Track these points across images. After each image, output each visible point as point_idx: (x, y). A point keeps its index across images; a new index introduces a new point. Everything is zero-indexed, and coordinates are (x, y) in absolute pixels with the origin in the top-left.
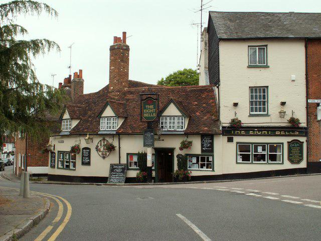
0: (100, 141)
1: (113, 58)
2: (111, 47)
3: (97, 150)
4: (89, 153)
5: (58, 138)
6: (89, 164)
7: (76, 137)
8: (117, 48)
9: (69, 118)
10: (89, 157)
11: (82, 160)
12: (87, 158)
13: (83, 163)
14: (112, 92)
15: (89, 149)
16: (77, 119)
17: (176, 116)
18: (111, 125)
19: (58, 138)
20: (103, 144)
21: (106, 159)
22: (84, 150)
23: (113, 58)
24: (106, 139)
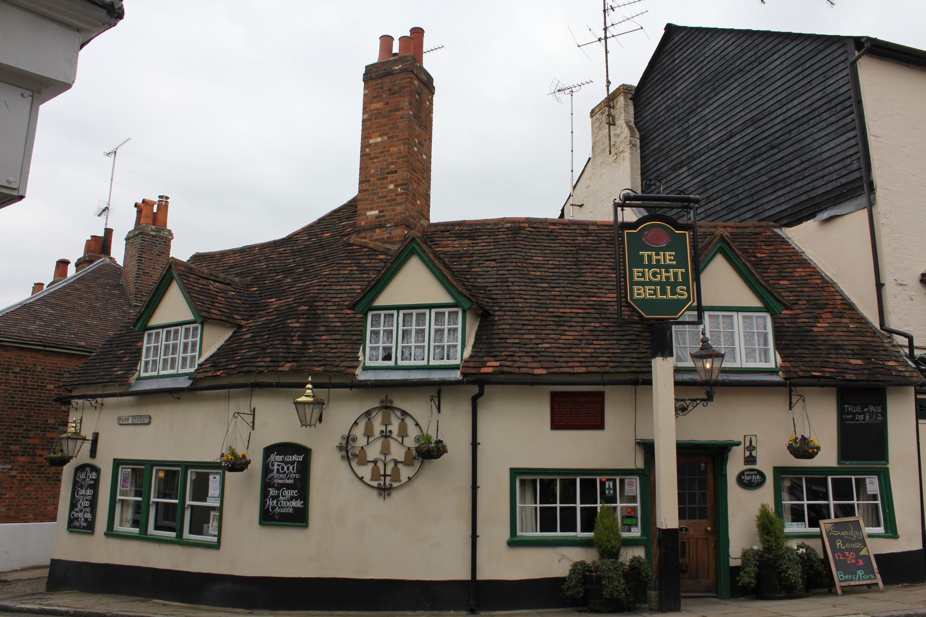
0: (368, 414)
1: (378, 105)
2: (369, 69)
3: (347, 458)
4: (304, 468)
5: (118, 406)
6: (299, 518)
7: (228, 397)
8: (403, 71)
9: (190, 317)
10: (302, 487)
11: (263, 503)
12: (288, 493)
13: (268, 518)
14: (373, 228)
15: (305, 451)
16: (221, 322)
17: (430, 307)
18: (180, 355)
19: (125, 408)
20: (378, 427)
21: (396, 495)
22: (276, 458)
23: (378, 105)
24: (398, 403)
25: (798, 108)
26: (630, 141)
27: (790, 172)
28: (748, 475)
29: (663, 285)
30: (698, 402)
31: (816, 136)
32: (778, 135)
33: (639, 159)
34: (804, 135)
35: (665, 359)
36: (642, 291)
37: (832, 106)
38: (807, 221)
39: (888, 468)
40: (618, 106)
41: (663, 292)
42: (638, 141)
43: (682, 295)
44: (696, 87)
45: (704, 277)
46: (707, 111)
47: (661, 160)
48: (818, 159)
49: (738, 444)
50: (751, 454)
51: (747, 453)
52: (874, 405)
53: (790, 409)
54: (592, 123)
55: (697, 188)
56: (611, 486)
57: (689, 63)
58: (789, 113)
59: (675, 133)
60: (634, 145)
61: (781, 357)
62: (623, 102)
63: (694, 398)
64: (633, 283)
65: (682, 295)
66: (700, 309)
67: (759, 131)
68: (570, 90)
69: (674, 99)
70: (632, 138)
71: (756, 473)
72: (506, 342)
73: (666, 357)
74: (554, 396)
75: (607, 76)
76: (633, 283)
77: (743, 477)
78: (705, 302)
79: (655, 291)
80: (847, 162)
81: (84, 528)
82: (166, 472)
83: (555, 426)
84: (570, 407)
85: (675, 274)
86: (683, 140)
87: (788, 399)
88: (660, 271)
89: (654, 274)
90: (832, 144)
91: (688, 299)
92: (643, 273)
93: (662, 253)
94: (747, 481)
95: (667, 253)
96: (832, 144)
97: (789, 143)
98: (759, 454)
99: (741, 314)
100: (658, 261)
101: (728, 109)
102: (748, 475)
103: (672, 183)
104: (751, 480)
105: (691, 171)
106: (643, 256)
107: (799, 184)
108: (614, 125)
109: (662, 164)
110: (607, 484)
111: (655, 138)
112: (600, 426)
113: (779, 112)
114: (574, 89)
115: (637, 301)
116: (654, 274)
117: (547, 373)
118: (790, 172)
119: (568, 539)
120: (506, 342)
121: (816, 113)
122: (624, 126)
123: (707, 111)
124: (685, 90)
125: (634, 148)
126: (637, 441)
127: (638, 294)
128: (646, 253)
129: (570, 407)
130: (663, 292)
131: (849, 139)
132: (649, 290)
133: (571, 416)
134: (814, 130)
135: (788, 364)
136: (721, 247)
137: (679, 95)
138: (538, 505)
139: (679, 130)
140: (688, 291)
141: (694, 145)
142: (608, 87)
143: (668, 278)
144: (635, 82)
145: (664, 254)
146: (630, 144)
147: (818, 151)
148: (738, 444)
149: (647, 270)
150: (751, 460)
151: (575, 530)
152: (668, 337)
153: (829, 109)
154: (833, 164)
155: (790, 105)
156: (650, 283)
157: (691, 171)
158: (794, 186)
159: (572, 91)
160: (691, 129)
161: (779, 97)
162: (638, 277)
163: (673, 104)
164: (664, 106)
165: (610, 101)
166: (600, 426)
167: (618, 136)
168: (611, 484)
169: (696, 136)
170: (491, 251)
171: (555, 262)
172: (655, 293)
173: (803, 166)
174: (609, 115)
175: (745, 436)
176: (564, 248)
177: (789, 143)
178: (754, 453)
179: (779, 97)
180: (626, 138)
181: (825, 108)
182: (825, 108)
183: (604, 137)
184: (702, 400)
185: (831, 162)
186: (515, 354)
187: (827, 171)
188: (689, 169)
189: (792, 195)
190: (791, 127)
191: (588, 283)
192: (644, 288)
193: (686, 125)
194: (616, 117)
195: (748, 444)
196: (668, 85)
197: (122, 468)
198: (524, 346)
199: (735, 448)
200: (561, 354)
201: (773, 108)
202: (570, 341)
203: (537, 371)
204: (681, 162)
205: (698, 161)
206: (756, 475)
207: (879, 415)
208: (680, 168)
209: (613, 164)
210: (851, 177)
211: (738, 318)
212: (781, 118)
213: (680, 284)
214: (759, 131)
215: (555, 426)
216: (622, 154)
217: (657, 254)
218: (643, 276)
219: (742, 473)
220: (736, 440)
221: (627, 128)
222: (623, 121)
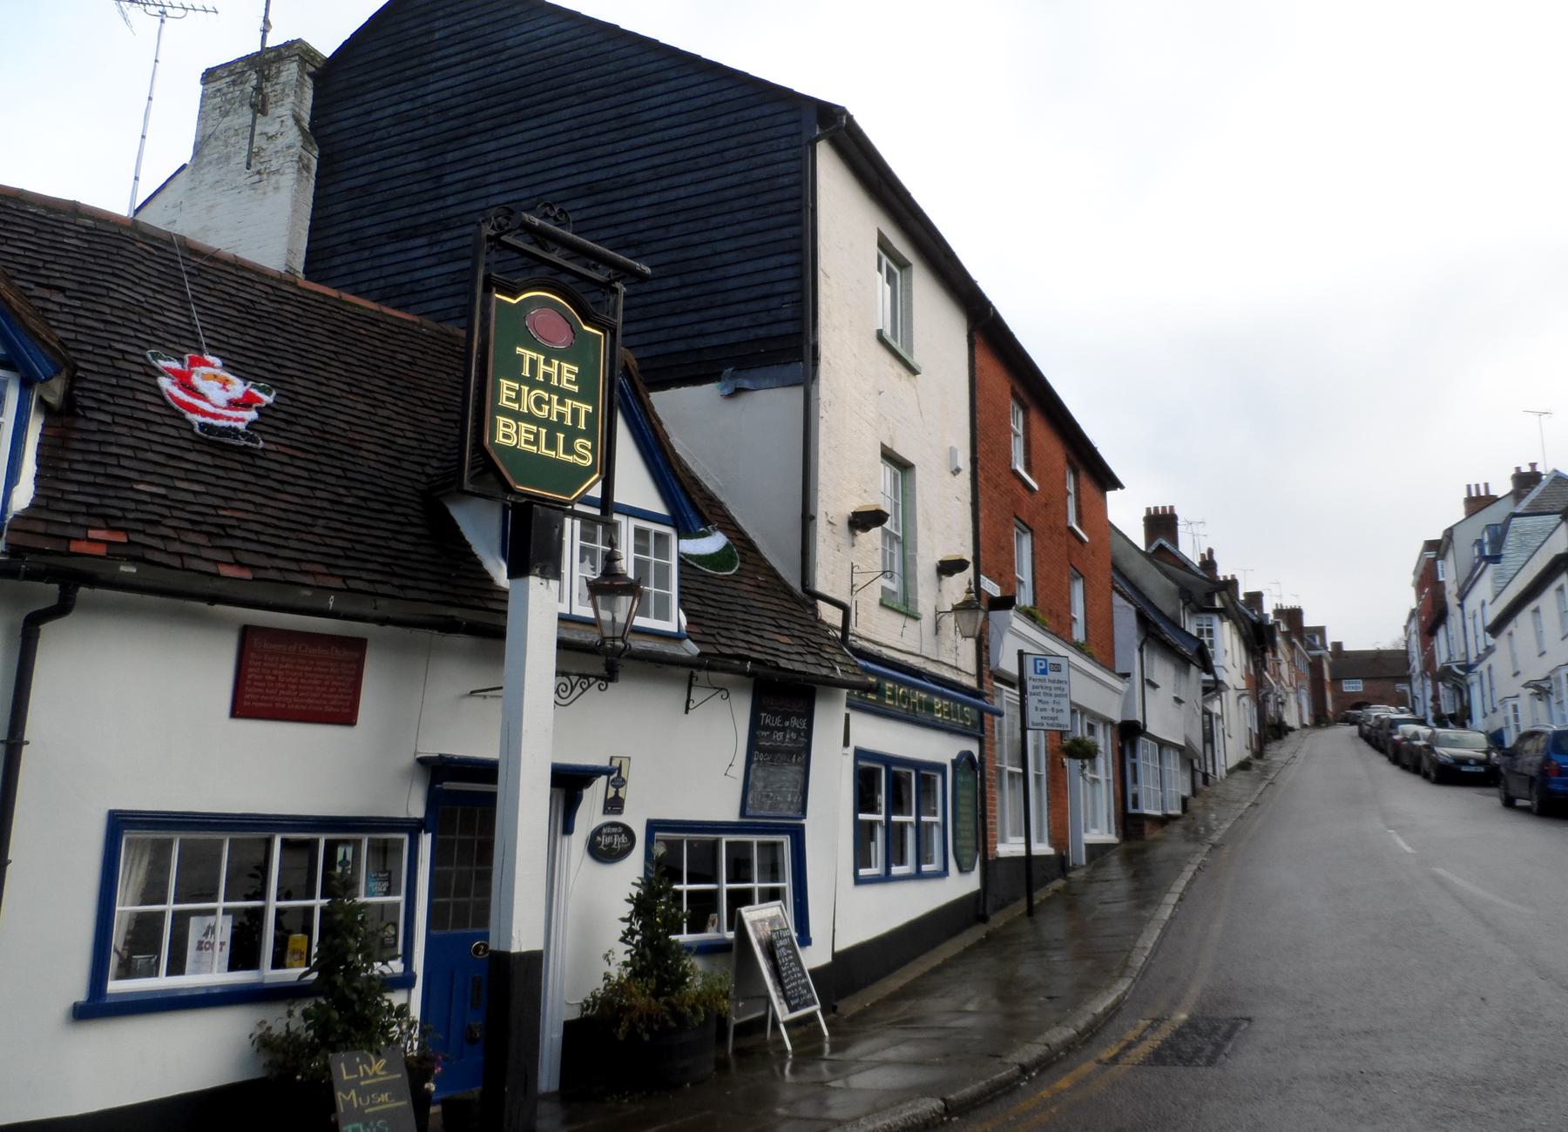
25: (692, 190)
26: (300, 157)
27: (657, 297)
28: (608, 835)
29: (553, 427)
30: (592, 680)
31: (719, 247)
32: (641, 226)
33: (312, 199)
34: (696, 238)
35: (544, 581)
36: (512, 431)
37: (758, 203)
38: (679, 386)
39: (803, 826)
40: (282, 79)
42: (315, 162)
43: (584, 458)
44: (473, 96)
46: (493, 145)
47: (364, 212)
48: (720, 286)
50: (617, 792)
51: (611, 793)
52: (798, 718)
53: (687, 712)
54: (203, 95)
55: (443, 283)
56: (349, 857)
57: (464, 46)
58: (672, 195)
59: (409, 168)
60: (307, 168)
62: (296, 76)
63: (587, 672)
65: (584, 458)
67: (603, 209)
68: (161, 8)
69: (418, 104)
70: (305, 153)
71: (620, 830)
72: (132, 489)
73: (547, 579)
74: (247, 635)
75: (267, 10)
77: (599, 838)
79: (537, 435)
80: (774, 302)
81: (940, 1064)
83: (242, 708)
85: (575, 412)
86: (426, 185)
87: (686, 693)
89: (539, 402)
90: (749, 267)
92: (519, 393)
93: (556, 362)
95: (566, 366)
96: (749, 267)
97: (662, 245)
98: (629, 794)
100: (547, 376)
101: (542, 153)
102: (608, 835)
103: (386, 260)
104: (611, 844)
105: (436, 249)
107: (672, 321)
108: (264, 113)
109: (367, 221)
110: (340, 851)
111: (357, 166)
112: (347, 717)
113: (650, 186)
114: (169, 11)
117: (254, 579)
118: (657, 297)
119: (197, 993)
120: (132, 489)
121: (726, 207)
122: (290, 122)
123: (493, 145)
124: (447, 93)
125: (305, 174)
127: (506, 436)
128: (528, 354)
130: (551, 444)
131: (783, 266)
134: (716, 234)
135: (696, 629)
137: (430, 99)
138: (221, 904)
139: (418, 166)
141: (450, 201)
142: (265, 32)
143: (561, 416)
144: (327, 46)
146: (297, 162)
147: (720, 272)
150: (614, 804)
152: (556, 538)
153: (753, 207)
154: (746, 301)
155: (677, 180)
156: (529, 418)
157: (436, 249)
158: (661, 322)
159: (163, 13)
160: (448, 169)
161: (657, 161)
163: (415, 112)
164: (390, 111)
165: (264, 63)
166: (347, 717)
167: (270, 138)
168: (350, 851)
169: (459, 187)
170: (48, 266)
172: (536, 442)
173: (684, 292)
174: (258, 89)
177: (662, 245)
179: (657, 161)
180: (289, 147)
181: (744, 202)
182: (744, 202)
183: (231, 132)
184: (598, 678)
185: (742, 295)
187: (733, 309)
188: (430, 245)
189: (655, 337)
190: (672, 219)
193: (438, 160)
194: (272, 100)
196: (408, 73)
201: (640, 176)
204: (415, 227)
205: (456, 233)
206: (620, 835)
207: (802, 734)
208: (411, 237)
209: (248, 192)
210: (776, 330)
212: (654, 198)
213: (583, 434)
214: (603, 209)
215: (242, 708)
216: (274, 178)
218: (518, 399)
219: (597, 832)
221: (296, 129)
222: (289, 112)
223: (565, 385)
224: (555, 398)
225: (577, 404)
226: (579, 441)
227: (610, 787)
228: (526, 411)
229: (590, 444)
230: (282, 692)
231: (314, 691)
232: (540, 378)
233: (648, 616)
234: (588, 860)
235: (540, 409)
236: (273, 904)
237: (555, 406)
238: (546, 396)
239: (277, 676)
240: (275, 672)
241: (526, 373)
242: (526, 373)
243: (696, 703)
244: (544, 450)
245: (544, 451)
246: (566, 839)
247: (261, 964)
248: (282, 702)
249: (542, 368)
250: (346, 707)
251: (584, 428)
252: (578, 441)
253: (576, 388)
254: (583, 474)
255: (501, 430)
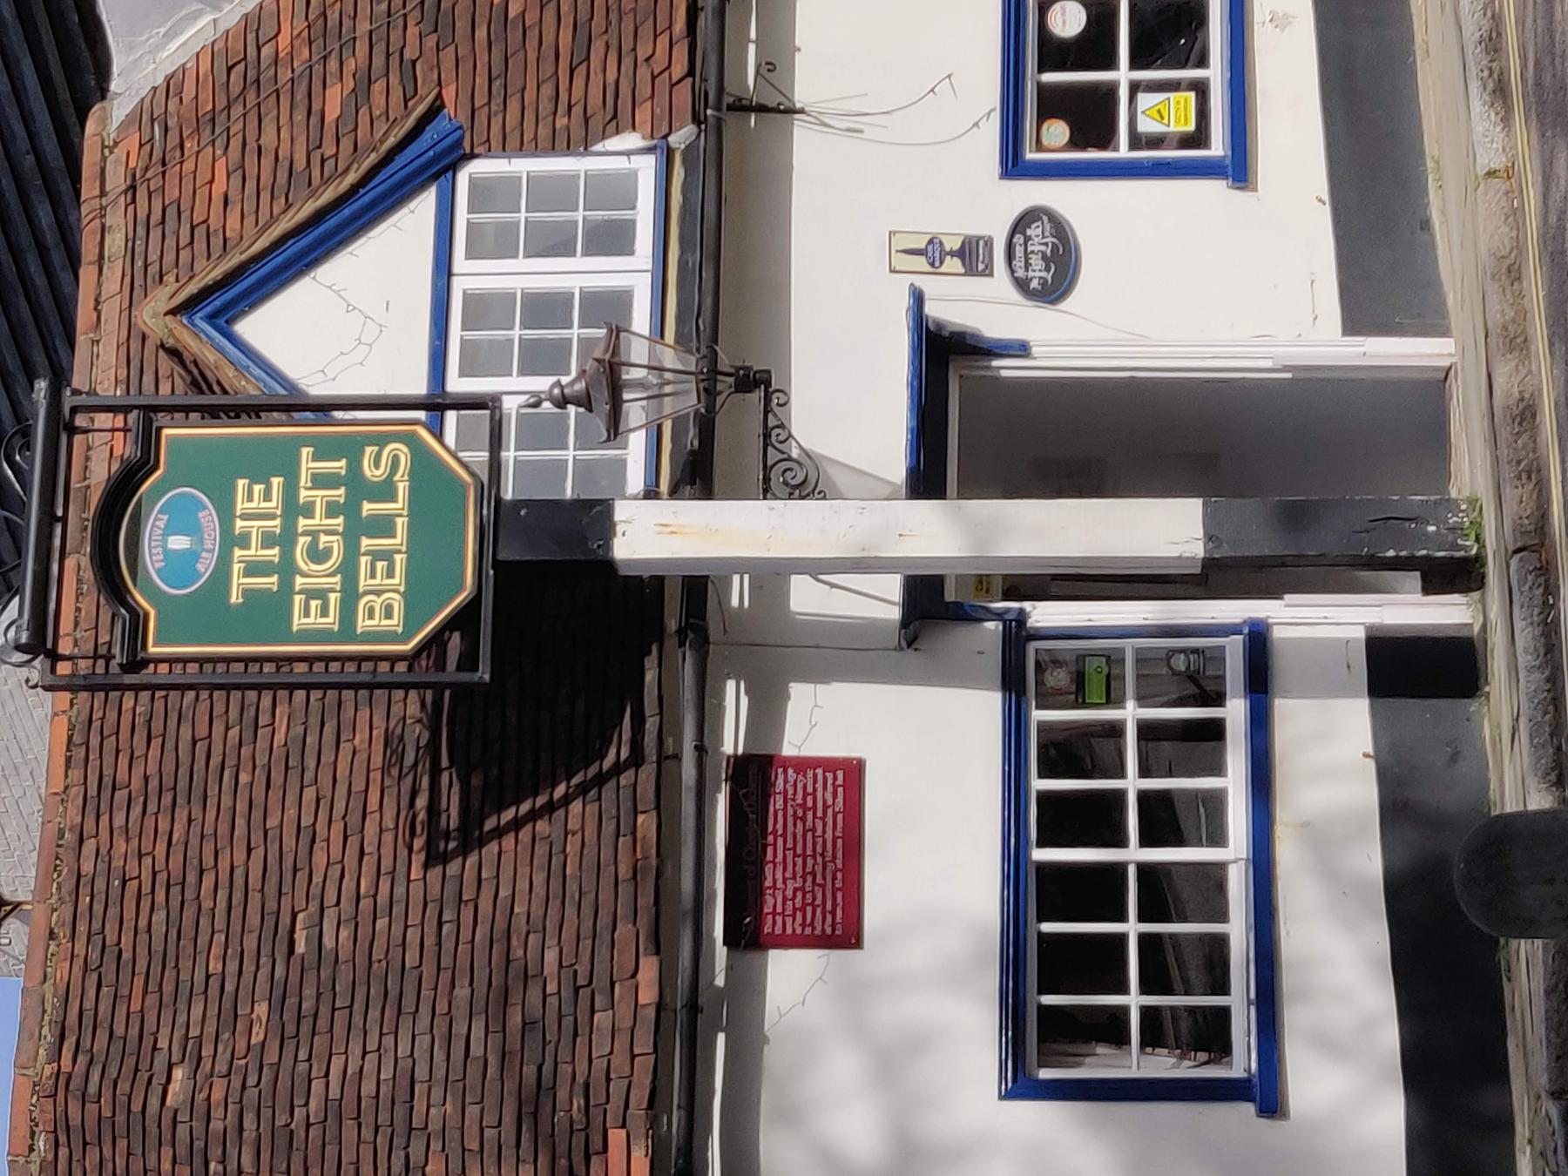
28: (1027, 266)
30: (772, 422)
36: (378, 602)
41: (383, 526)
45: (317, 387)
49: (918, 298)
50: (952, 254)
51: (953, 264)
61: (617, 132)
64: (347, 629)
66: (437, 404)
71: (1019, 239)
76: (347, 629)
77: (1034, 284)
78: (418, 386)
79: (377, 555)
82: (1043, 115)
84: (779, 876)
85: (320, 481)
88: (305, 533)
89: (317, 555)
91: (412, 441)
92: (311, 594)
93: (239, 523)
94: (1047, 269)
95: (241, 505)
98: (954, 228)
99: (460, 263)
100: (268, 540)
102: (1027, 266)
104: (1044, 257)
106: (248, 593)
115: (412, 620)
116: (317, 555)
126: (904, 644)
128: (239, 583)
129: (779, 876)
130: (383, 526)
132: (373, 576)
133: (814, 874)
135: (643, 114)
136: (211, 318)
140: (381, 441)
143: (332, 510)
145: (245, 517)
148: (918, 298)
149: (299, 580)
150: (972, 256)
151: (1221, 867)
156: (348, 570)
162: (324, 613)
166: (851, 774)
171: (216, 950)
172: (387, 555)
175: (893, 271)
176: (159, 916)
178: (953, 244)
186: (580, 1080)
191: (306, 821)
192: (367, 593)
195: (921, 263)
197: (1039, 146)
198: (550, 1049)
199: (932, 310)
200: (587, 910)
202: (539, 878)
203: (648, 995)
211: (471, 275)
217: (244, 540)
218: (321, 594)
219: (1022, 285)
220: (904, 302)
223: (275, 503)
224: (302, 523)
225: (304, 479)
226: (368, 470)
227: (942, 270)
228: (337, 579)
229: (368, 450)
230: (819, 880)
231: (814, 830)
232: (274, 553)
233: (633, 223)
234: (1068, 304)
235: (327, 553)
236: (1134, 853)
237: (316, 521)
238: (303, 541)
239: (795, 890)
240: (789, 893)
241: (271, 582)
242: (271, 582)
243: (782, 99)
244: (398, 541)
245: (400, 538)
246: (1035, 350)
247: (1209, 62)
248: (834, 878)
249: (255, 552)
250: (835, 778)
251: (343, 463)
252: (367, 473)
253: (276, 481)
254: (424, 464)
255: (378, 623)
